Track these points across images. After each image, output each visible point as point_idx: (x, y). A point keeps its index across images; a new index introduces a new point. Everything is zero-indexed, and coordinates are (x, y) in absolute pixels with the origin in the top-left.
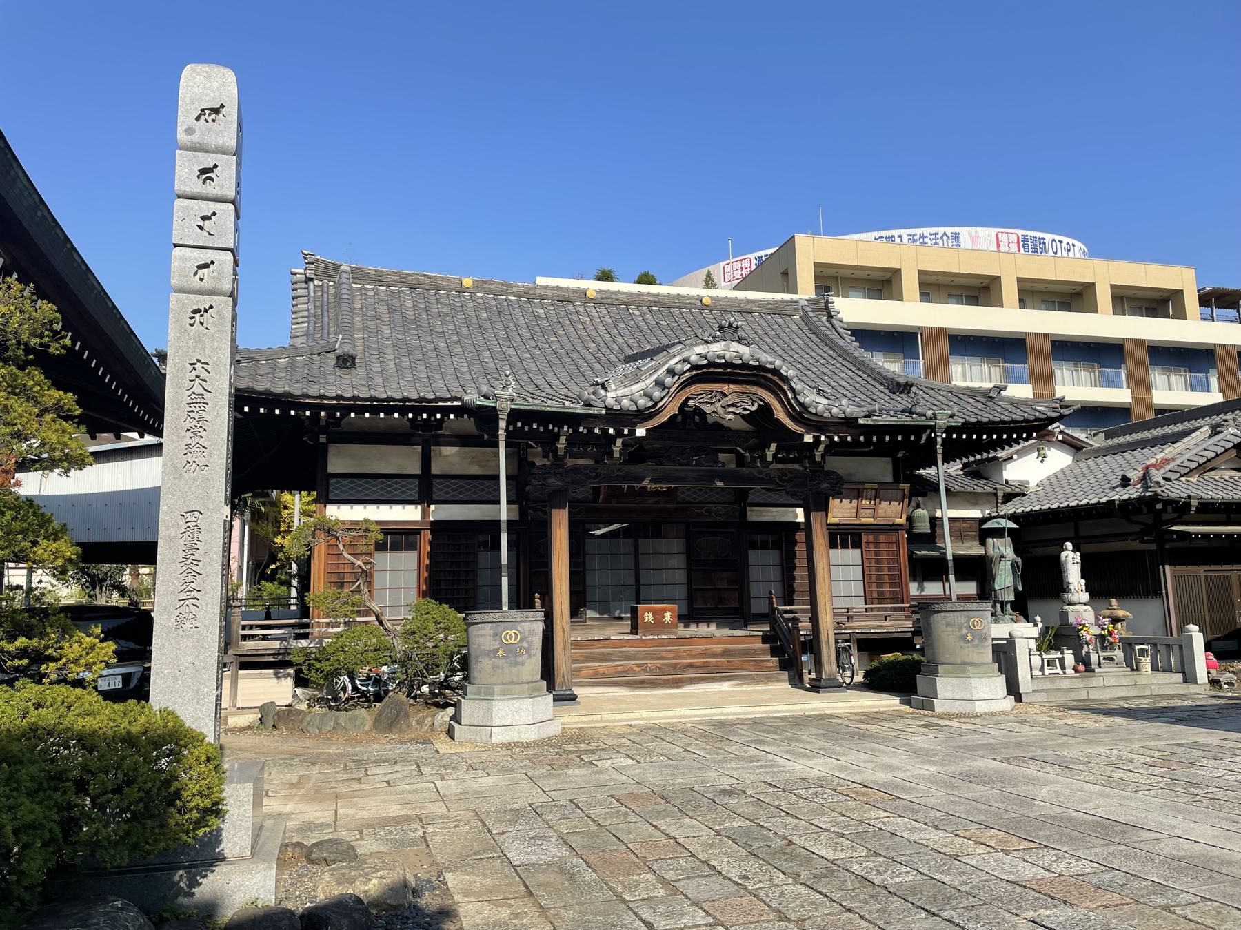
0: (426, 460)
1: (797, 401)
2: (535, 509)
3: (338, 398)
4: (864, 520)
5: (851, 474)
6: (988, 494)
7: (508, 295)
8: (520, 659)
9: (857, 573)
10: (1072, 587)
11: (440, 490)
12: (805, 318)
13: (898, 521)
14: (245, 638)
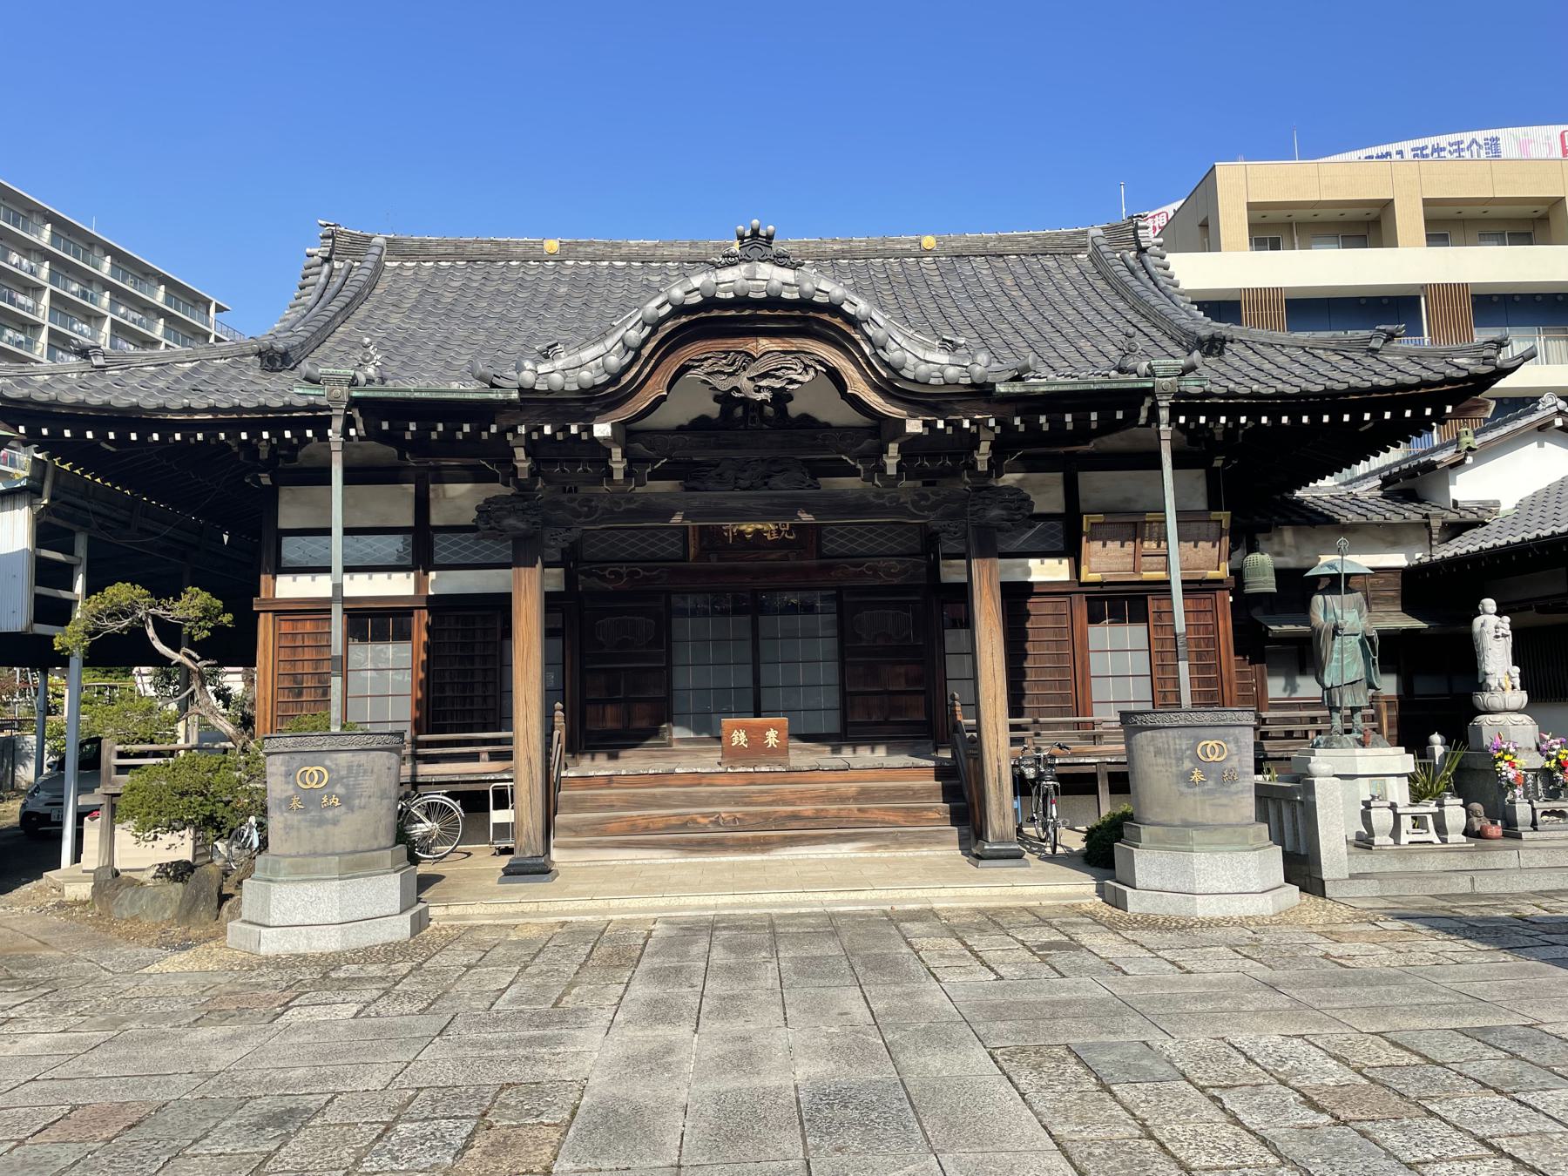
0: (422, 506)
1: (881, 360)
2: (589, 574)
3: (212, 409)
4: (1147, 576)
5: (1128, 500)
6: (1418, 524)
7: (611, 259)
8: (329, 814)
10: (1492, 682)
11: (445, 549)
12: (1096, 258)
13: (1212, 574)
14: (122, 769)
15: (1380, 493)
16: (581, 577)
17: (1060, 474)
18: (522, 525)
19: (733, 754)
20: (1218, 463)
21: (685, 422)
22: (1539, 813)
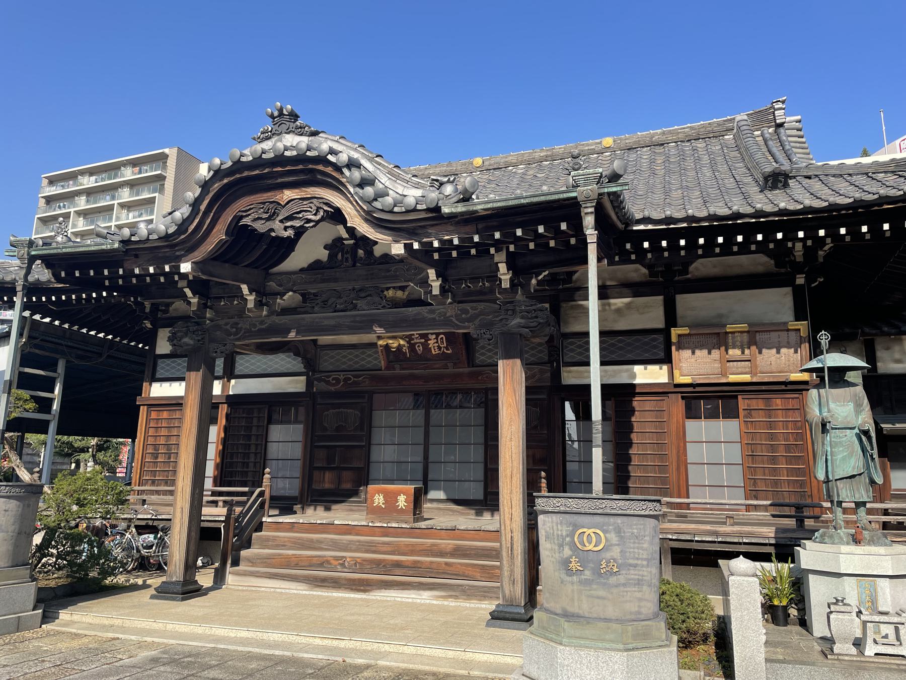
4: (733, 378)
9: (735, 453)
16: (315, 382)
17: (661, 297)
18: (191, 342)
20: (800, 280)
21: (306, 266)
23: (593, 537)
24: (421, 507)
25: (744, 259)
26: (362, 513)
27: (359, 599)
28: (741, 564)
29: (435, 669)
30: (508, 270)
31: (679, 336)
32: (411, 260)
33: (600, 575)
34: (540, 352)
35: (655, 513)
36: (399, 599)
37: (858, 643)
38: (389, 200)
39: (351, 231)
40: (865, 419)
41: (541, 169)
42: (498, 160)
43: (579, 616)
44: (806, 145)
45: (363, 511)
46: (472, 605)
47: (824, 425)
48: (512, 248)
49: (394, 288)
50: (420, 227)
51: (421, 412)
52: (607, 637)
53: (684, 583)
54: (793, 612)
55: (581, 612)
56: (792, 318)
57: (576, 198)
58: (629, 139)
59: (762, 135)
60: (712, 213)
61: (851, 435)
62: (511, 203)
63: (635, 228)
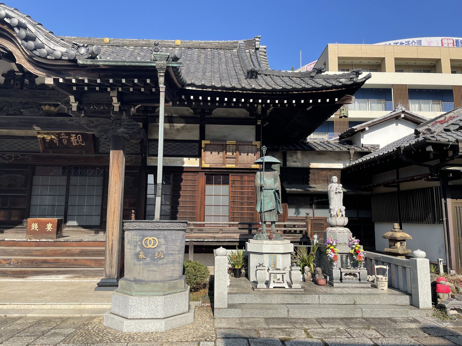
4: (228, 166)
6: (345, 152)
9: (226, 201)
15: (338, 141)
17: (199, 125)
19: (34, 233)
22: (343, 274)
23: (152, 241)
24: (61, 230)
25: (236, 110)
26: (23, 234)
27: (19, 282)
28: (221, 251)
29: (62, 315)
30: (118, 101)
31: (206, 144)
32: (57, 88)
33: (154, 260)
34: (136, 148)
35: (184, 228)
36: (45, 280)
37: (267, 283)
38: (44, 51)
39: (20, 67)
40: (278, 185)
41: (142, 50)
42: (118, 41)
43: (142, 281)
44: (267, 60)
45: (25, 233)
46: (88, 280)
47: (261, 188)
48: (120, 89)
49: (49, 105)
50: (64, 70)
51: (65, 178)
52: (155, 290)
53: (197, 262)
54: (243, 271)
55: (143, 279)
56: (254, 140)
57: (155, 67)
58: (189, 43)
59: (249, 52)
60: (223, 85)
61: (272, 192)
62: (119, 64)
63: (187, 88)
